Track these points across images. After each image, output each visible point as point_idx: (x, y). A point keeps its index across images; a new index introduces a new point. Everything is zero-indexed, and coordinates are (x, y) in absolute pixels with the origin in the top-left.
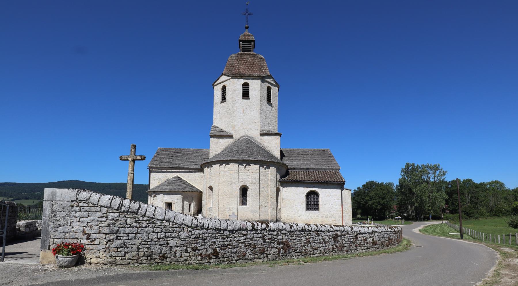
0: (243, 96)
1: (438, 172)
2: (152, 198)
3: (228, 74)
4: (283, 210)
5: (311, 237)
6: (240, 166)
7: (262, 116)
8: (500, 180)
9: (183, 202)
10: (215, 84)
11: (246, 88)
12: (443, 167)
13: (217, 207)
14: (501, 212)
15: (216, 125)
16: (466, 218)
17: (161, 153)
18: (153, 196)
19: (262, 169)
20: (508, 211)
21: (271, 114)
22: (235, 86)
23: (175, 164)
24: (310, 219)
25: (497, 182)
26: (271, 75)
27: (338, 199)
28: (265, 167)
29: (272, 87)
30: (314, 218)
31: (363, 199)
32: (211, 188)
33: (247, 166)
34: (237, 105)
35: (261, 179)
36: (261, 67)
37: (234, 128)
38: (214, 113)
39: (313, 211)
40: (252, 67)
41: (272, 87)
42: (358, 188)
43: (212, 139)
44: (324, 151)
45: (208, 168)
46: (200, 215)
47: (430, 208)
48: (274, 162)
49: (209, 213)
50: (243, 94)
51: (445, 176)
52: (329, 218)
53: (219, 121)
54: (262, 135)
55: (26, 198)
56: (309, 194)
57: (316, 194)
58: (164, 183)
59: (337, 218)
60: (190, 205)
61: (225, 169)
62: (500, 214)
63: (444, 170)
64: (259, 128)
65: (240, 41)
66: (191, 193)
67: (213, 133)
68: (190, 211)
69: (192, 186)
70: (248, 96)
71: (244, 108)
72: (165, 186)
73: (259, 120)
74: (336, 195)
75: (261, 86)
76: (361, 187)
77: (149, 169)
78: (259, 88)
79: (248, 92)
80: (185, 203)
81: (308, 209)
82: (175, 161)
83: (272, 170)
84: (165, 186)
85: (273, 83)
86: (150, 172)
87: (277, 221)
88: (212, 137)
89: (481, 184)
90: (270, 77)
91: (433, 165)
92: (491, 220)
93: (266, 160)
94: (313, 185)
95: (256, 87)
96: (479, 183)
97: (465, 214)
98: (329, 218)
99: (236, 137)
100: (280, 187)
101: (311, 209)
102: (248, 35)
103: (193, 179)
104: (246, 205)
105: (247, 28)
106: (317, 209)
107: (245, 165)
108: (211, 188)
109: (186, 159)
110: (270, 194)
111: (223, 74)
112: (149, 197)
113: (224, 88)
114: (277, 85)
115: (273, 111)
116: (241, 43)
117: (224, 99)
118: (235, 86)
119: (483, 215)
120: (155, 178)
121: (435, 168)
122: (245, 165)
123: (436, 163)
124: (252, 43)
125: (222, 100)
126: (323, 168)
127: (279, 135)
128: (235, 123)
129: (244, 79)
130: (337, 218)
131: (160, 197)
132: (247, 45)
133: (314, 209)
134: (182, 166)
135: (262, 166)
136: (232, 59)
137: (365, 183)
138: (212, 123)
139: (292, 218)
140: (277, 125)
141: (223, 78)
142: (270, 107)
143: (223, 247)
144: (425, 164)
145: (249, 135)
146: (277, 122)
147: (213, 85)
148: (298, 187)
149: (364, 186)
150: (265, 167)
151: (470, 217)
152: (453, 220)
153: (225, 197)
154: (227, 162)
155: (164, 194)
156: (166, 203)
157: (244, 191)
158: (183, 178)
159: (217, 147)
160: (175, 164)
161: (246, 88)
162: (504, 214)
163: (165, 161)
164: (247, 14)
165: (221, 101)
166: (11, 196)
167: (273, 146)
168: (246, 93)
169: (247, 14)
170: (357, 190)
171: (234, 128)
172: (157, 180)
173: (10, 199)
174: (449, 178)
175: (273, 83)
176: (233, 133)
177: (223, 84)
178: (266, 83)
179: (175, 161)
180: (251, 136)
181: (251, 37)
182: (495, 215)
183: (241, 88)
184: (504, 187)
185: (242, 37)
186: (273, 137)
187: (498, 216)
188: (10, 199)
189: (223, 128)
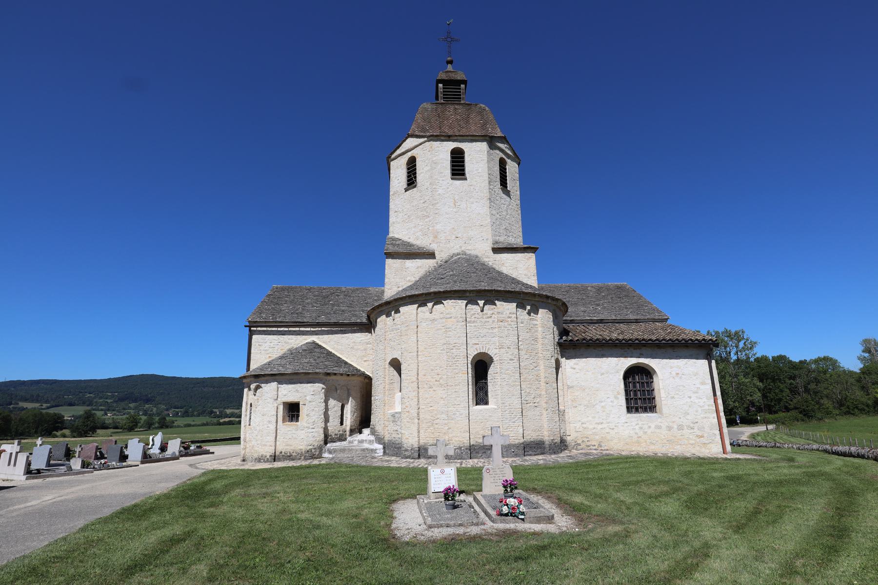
0: (453, 174)
1: (741, 344)
2: (252, 392)
3: (417, 133)
4: (570, 414)
6: (470, 306)
7: (494, 212)
8: (831, 355)
9: (326, 402)
10: (393, 156)
11: (458, 158)
12: (751, 334)
13: (414, 412)
14: (857, 408)
15: (397, 236)
16: (803, 420)
17: (275, 298)
18: (253, 386)
19: (523, 314)
20: (868, 406)
22: (434, 156)
23: (307, 315)
24: (641, 433)
25: (826, 359)
26: (505, 138)
27: (703, 383)
28: (528, 307)
29: (508, 161)
30: (649, 431)
32: (396, 365)
33: (486, 307)
34: (440, 191)
35: (518, 337)
37: (436, 237)
38: (391, 213)
39: (644, 415)
40: (467, 122)
41: (508, 161)
43: (389, 262)
44: (618, 288)
45: (388, 315)
46: (366, 431)
47: (737, 404)
49: (391, 427)
50: (453, 170)
51: (755, 350)
52: (686, 431)
53: (403, 224)
54: (496, 250)
55: (71, 404)
56: (630, 373)
57: (646, 373)
58: (281, 358)
61: (432, 316)
62: (856, 410)
63: (754, 340)
64: (490, 237)
65: (439, 81)
66: (345, 377)
67: (391, 249)
68: (342, 424)
69: (346, 363)
70: (464, 174)
71: (457, 197)
72: (283, 362)
74: (696, 374)
75: (489, 154)
77: (250, 327)
78: (485, 158)
79: (463, 166)
80: (332, 402)
81: (629, 409)
82: (308, 311)
83: (544, 317)
84: (283, 362)
85: (509, 152)
88: (390, 255)
89: (801, 362)
90: (503, 139)
91: (733, 331)
92: (843, 421)
94: (638, 351)
95: (477, 154)
96: (797, 361)
97: (801, 413)
98: (686, 431)
99: (442, 255)
101: (637, 411)
103: (349, 348)
104: (487, 403)
105: (451, 62)
107: (481, 303)
108: (396, 365)
109: (333, 305)
110: (542, 375)
112: (246, 390)
113: (412, 165)
114: (517, 159)
115: (512, 206)
116: (441, 85)
117: (412, 181)
118: (434, 156)
119: (828, 413)
120: (262, 348)
121: (737, 336)
122: (481, 303)
123: (738, 329)
124: (463, 86)
125: (409, 185)
127: (532, 250)
129: (454, 141)
131: (269, 389)
132: (452, 85)
133: (645, 410)
134: (323, 319)
136: (426, 109)
138: (388, 233)
139: (595, 434)
140: (521, 234)
141: (410, 143)
142: (508, 199)
144: (721, 330)
145: (468, 252)
146: (521, 229)
147: (389, 160)
148: (603, 356)
150: (528, 307)
151: (809, 417)
152: (783, 423)
154: (438, 297)
155: (280, 383)
156: (285, 404)
157: (481, 367)
159: (400, 276)
160: (307, 315)
161: (458, 158)
162: (862, 411)
163: (286, 312)
165: (405, 186)
166: (46, 402)
167: (523, 269)
168: (458, 167)
169: (449, 40)
171: (436, 237)
172: (268, 349)
173: (45, 405)
174: (760, 351)
175: (509, 152)
176: (433, 247)
177: (409, 154)
178: (498, 152)
179: (308, 311)
180: (473, 253)
181: (460, 76)
182: (848, 413)
184: (839, 367)
185: (442, 76)
186: (519, 256)
187: (853, 414)
188: (45, 405)
189: (412, 240)
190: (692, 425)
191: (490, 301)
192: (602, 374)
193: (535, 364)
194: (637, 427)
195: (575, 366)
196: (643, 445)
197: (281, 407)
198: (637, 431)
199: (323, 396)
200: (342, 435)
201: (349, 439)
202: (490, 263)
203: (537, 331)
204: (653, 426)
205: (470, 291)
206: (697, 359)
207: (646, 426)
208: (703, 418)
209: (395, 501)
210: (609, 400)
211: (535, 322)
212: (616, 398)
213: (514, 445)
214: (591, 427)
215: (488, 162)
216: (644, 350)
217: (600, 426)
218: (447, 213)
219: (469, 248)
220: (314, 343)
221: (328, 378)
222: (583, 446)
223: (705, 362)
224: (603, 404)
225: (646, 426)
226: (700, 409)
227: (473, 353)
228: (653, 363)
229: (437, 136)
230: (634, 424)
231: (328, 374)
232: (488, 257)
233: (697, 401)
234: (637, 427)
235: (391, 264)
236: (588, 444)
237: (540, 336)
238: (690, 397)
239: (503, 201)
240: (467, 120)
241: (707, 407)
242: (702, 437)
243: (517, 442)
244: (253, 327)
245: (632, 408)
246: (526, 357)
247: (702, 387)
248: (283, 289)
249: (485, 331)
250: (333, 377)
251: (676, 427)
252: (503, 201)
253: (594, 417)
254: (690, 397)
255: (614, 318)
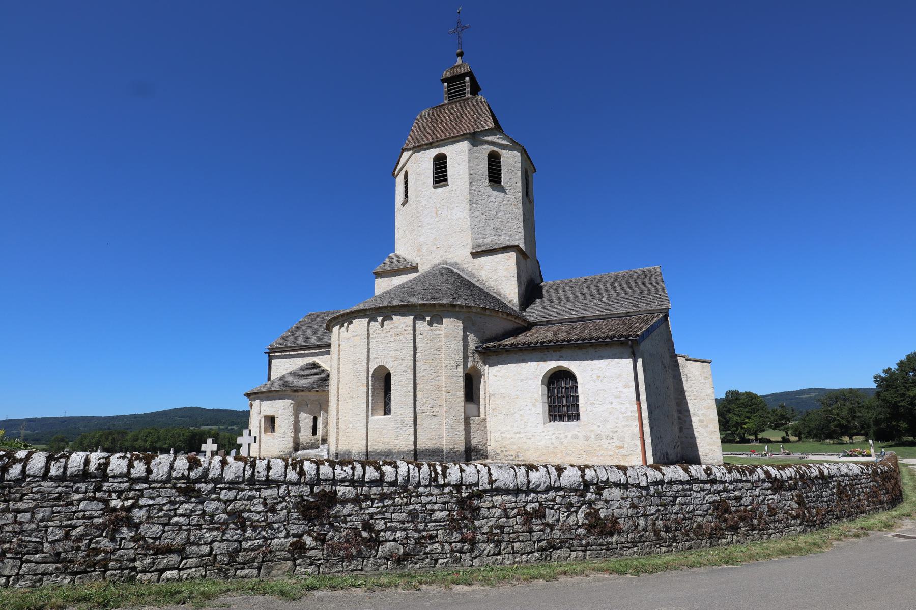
0: (436, 182)
5: (142, 501)
6: (372, 323)
7: (477, 214)
11: (440, 164)
15: (403, 255)
19: (422, 326)
21: (502, 208)
24: (557, 444)
27: (626, 386)
28: (428, 319)
30: (566, 441)
31: (903, 395)
34: (423, 203)
36: (478, 118)
37: (419, 250)
42: (884, 371)
44: (645, 274)
48: (454, 306)
52: (604, 441)
54: (476, 255)
57: (569, 376)
59: (627, 440)
60: (315, 420)
65: (444, 81)
70: (446, 180)
73: (468, 224)
76: (894, 367)
78: (466, 158)
80: (303, 416)
83: (451, 327)
86: (271, 358)
87: (470, 453)
93: (432, 301)
94: (558, 354)
95: (459, 156)
98: (604, 441)
99: (422, 269)
100: (480, 365)
102: (461, 65)
105: (461, 55)
106: (577, 417)
111: (404, 150)
114: (515, 145)
116: (446, 84)
124: (467, 79)
126: (622, 310)
128: (422, 239)
130: (627, 440)
133: (550, 415)
135: (419, 317)
137: (904, 358)
139: (512, 444)
142: (501, 195)
143: (329, 514)
145: (449, 261)
148: (523, 361)
149: (901, 364)
150: (428, 319)
153: (379, 397)
155: (262, 400)
158: (323, 365)
161: (440, 164)
164: (459, 29)
168: (440, 174)
170: (883, 375)
171: (419, 250)
176: (417, 260)
178: (486, 146)
180: (454, 260)
183: (448, 169)
186: (499, 257)
190: (611, 434)
191: (387, 317)
192: (522, 380)
193: (435, 375)
194: (553, 437)
195: (498, 374)
196: (559, 456)
197: (263, 420)
198: (554, 441)
199: (291, 409)
200: (314, 444)
201: (321, 447)
202: (470, 269)
203: (440, 341)
204: (570, 436)
205: (370, 309)
206: (622, 358)
207: (562, 436)
208: (624, 426)
209: (18, 480)
210: (527, 408)
211: (438, 332)
212: (534, 405)
213: (404, 452)
214: (509, 436)
215: (470, 161)
216: (564, 352)
217: (518, 436)
218: (429, 224)
219: (450, 256)
220: (314, 365)
221: (296, 394)
222: (501, 456)
223: (629, 361)
224: (521, 412)
225: (562, 436)
226: (621, 416)
227: (373, 367)
228: (574, 366)
229: (431, 144)
230: (550, 433)
231: (296, 391)
232: (467, 263)
233: (618, 407)
234: (553, 437)
235: (378, 281)
236: (506, 454)
237: (443, 344)
238: (612, 403)
239: (492, 199)
240: (460, 119)
241: (629, 414)
242: (622, 447)
243: (407, 449)
244: (272, 353)
245: (555, 416)
246: (425, 367)
247: (625, 391)
248: (314, 316)
249: (384, 345)
250: (302, 394)
251: (593, 436)
252: (492, 199)
253: (512, 426)
254: (612, 403)
255: (598, 313)
